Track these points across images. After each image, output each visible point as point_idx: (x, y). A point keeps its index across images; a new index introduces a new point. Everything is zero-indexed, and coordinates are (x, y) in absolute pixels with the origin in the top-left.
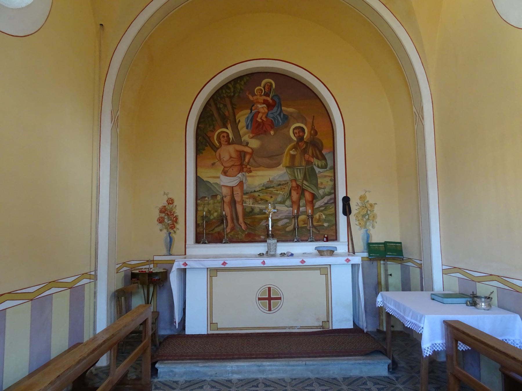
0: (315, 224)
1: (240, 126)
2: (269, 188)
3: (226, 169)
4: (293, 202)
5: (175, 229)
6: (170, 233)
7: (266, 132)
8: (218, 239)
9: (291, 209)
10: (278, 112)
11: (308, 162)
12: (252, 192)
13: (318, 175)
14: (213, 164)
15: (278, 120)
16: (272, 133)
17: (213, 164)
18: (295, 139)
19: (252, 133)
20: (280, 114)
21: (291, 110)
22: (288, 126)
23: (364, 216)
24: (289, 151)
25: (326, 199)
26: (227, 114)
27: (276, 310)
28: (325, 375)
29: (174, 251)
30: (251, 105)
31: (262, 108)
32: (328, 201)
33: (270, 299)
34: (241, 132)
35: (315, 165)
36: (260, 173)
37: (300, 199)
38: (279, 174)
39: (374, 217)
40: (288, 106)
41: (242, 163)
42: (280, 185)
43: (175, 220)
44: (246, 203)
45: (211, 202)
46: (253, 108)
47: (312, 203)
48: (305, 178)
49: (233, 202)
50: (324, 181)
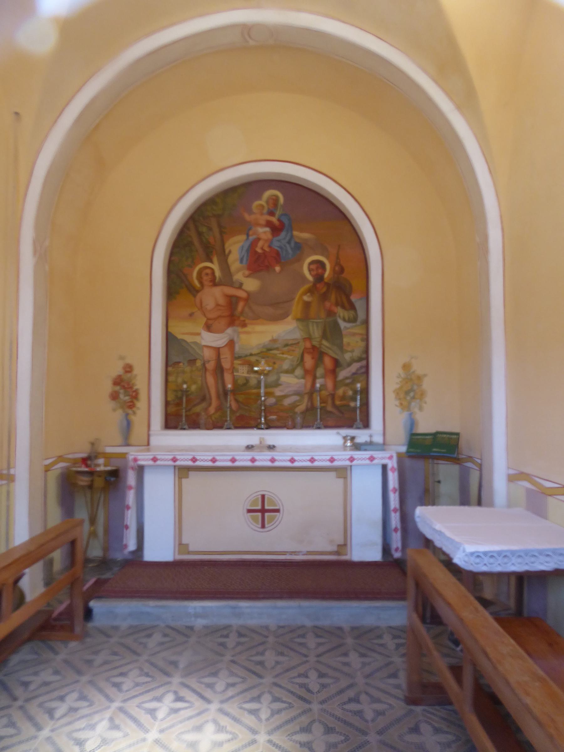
0: (338, 403)
1: (231, 259)
2: (271, 350)
3: (210, 322)
4: (306, 372)
5: (134, 409)
6: (127, 415)
7: (268, 268)
8: (194, 424)
9: (303, 381)
10: (288, 238)
11: (330, 313)
12: (246, 356)
13: (344, 332)
14: (191, 315)
15: (287, 251)
16: (278, 269)
17: (191, 315)
18: (310, 278)
19: (249, 268)
20: (289, 242)
21: (305, 235)
22: (299, 260)
23: (407, 393)
24: (302, 296)
25: (354, 367)
26: (212, 241)
27: (275, 525)
28: (325, 623)
29: (133, 439)
30: (246, 228)
31: (264, 232)
32: (357, 370)
33: (263, 511)
34: (233, 268)
35: (340, 317)
36: (259, 328)
37: (316, 366)
38: (286, 329)
39: (423, 394)
40: (301, 231)
41: (233, 314)
42: (287, 345)
43: (135, 396)
44: (238, 372)
45: (188, 369)
46: (251, 233)
47: (334, 372)
48: (324, 336)
49: (219, 370)
50: (351, 341)
